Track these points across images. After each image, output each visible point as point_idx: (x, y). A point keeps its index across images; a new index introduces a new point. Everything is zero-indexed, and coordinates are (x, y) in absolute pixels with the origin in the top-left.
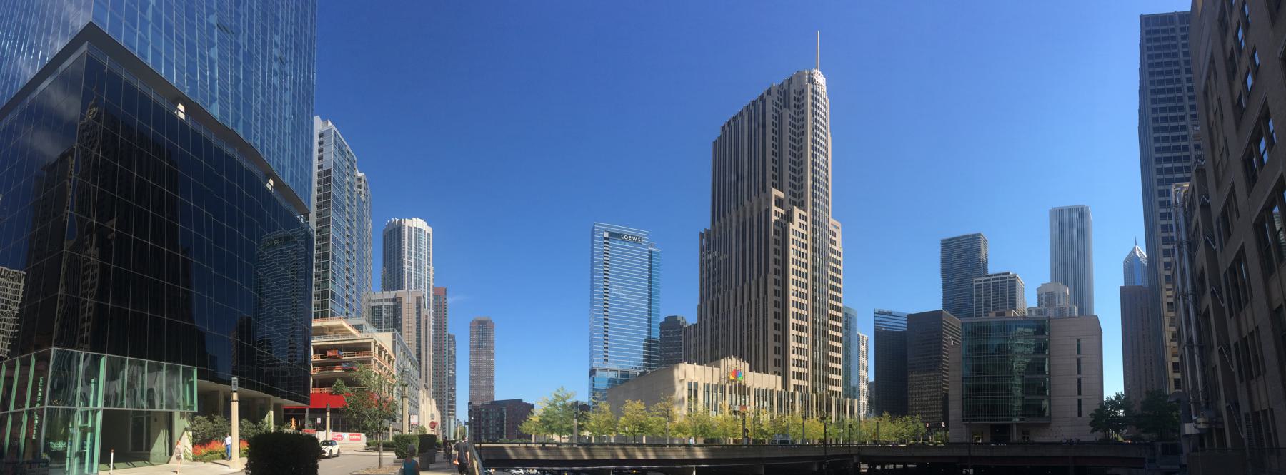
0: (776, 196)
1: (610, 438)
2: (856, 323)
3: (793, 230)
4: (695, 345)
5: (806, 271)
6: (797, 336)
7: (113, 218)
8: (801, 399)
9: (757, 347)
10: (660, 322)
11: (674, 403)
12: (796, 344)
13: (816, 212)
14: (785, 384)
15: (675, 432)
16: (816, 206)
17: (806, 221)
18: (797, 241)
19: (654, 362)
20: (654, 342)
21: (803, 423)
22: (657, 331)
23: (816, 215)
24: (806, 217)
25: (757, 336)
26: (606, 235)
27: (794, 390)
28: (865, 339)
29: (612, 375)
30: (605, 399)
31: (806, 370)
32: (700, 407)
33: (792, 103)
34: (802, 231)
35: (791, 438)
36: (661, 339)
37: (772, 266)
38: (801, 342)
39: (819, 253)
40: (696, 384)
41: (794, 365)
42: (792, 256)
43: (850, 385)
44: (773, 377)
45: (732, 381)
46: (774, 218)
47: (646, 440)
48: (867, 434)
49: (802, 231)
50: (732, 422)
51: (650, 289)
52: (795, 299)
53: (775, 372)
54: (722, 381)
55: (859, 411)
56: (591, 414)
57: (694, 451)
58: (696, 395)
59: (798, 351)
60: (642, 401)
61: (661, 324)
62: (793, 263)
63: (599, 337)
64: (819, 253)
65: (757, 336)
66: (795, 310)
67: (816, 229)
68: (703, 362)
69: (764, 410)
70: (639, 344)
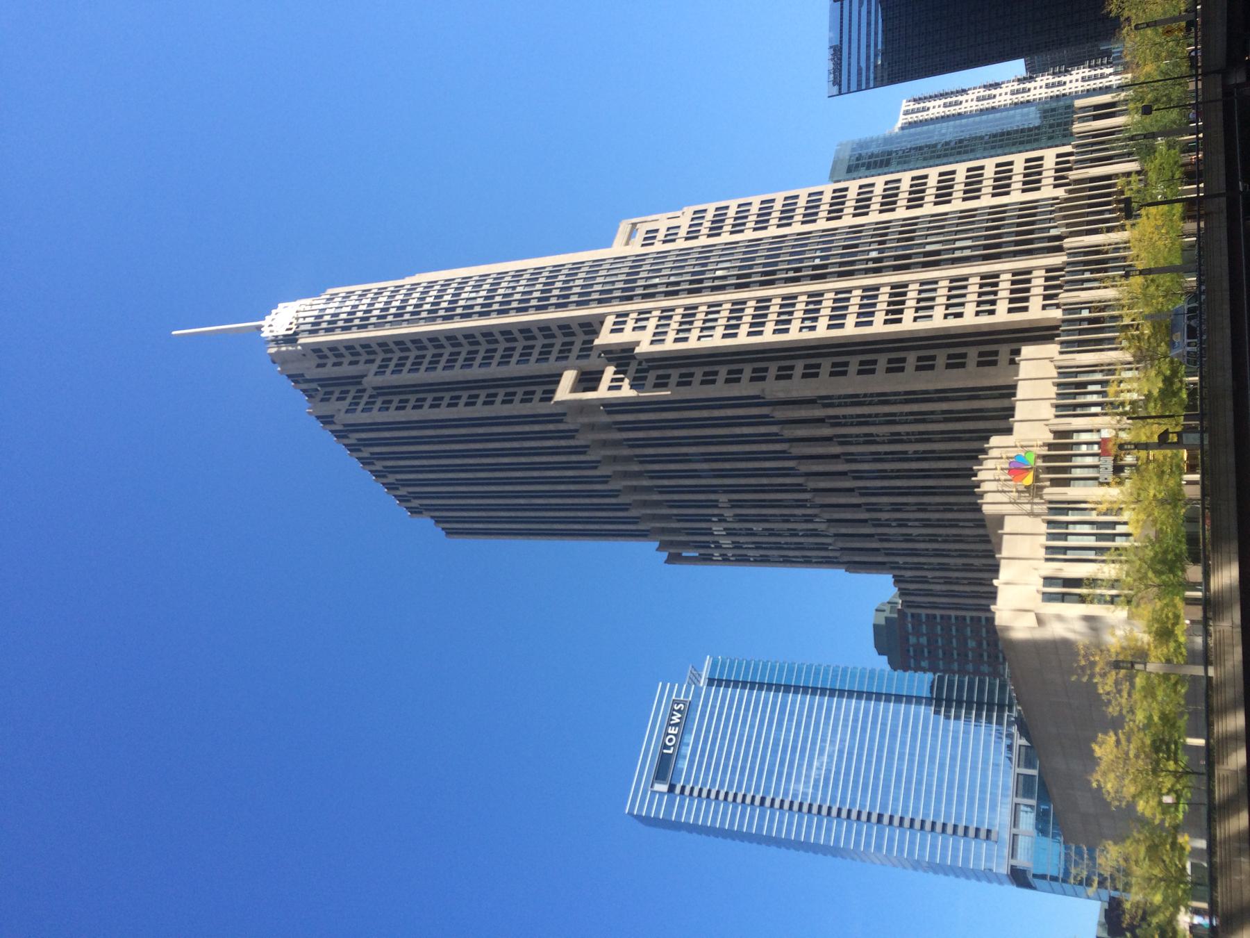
0: (574, 389)
1: (1195, 852)
2: (872, 141)
3: (652, 342)
4: (948, 581)
5: (753, 303)
6: (917, 310)
8: (1079, 284)
9: (950, 416)
10: (888, 668)
11: (1099, 647)
12: (939, 312)
13: (601, 292)
14: (1041, 334)
15: (1172, 645)
16: (589, 294)
17: (626, 315)
18: (679, 331)
19: (991, 692)
20: (940, 688)
21: (1142, 272)
22: (911, 681)
23: (610, 291)
24: (618, 315)
25: (921, 418)
26: (664, 788)
27: (1058, 306)
28: (912, 106)
29: (1028, 820)
30: (1091, 851)
31: (1003, 277)
32: (1108, 571)
33: (346, 370)
34: (652, 324)
35: (1182, 303)
36: (933, 669)
37: (745, 388)
38: (933, 299)
39: (703, 273)
40: (1049, 581)
41: (992, 312)
42: (717, 340)
43: (1038, 128)
44: (1025, 369)
45: (1037, 479)
46: (627, 391)
47: (1197, 736)
48: (1172, 54)
49: (652, 324)
50: (1142, 478)
51: (805, 690)
52: (823, 323)
53: (1012, 362)
54: (1037, 509)
55: (1107, 90)
56: (1133, 898)
57: (1221, 593)
58: (1077, 582)
59: (954, 306)
60: (1094, 740)
61: (894, 665)
62: (735, 335)
63: (926, 846)
64: (703, 273)
65: (921, 418)
66: (851, 320)
67: (646, 287)
68: (990, 561)
69: (1111, 389)
70: (946, 730)
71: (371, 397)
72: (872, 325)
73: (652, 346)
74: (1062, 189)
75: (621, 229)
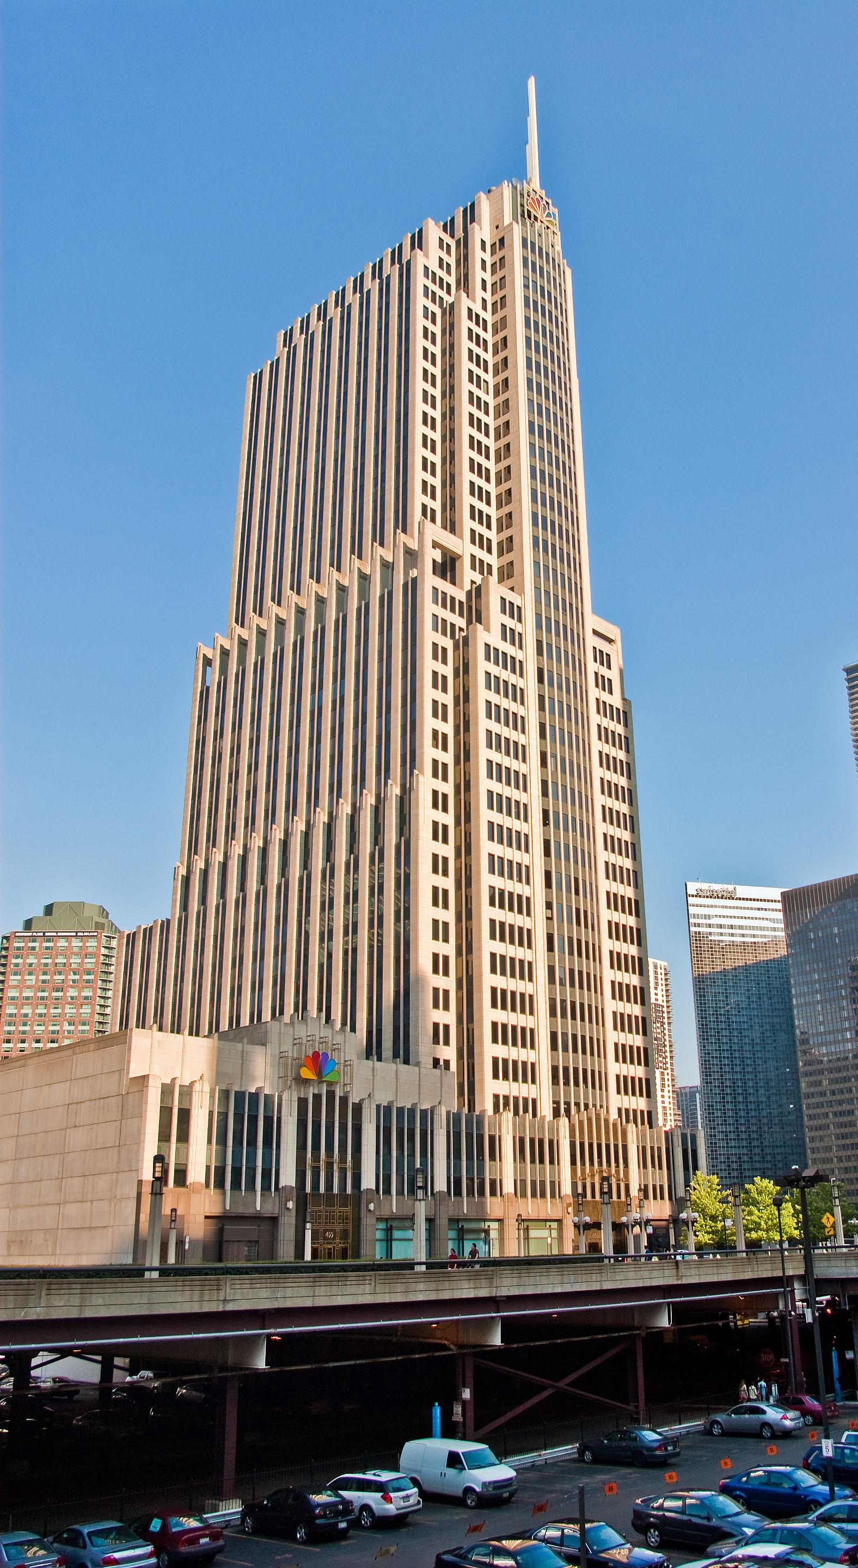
3: (487, 646)
7: (502, 1453)
63: (61, 1164)
71: (441, 299)
72: (488, 808)
73: (487, 823)
74: (616, 1116)
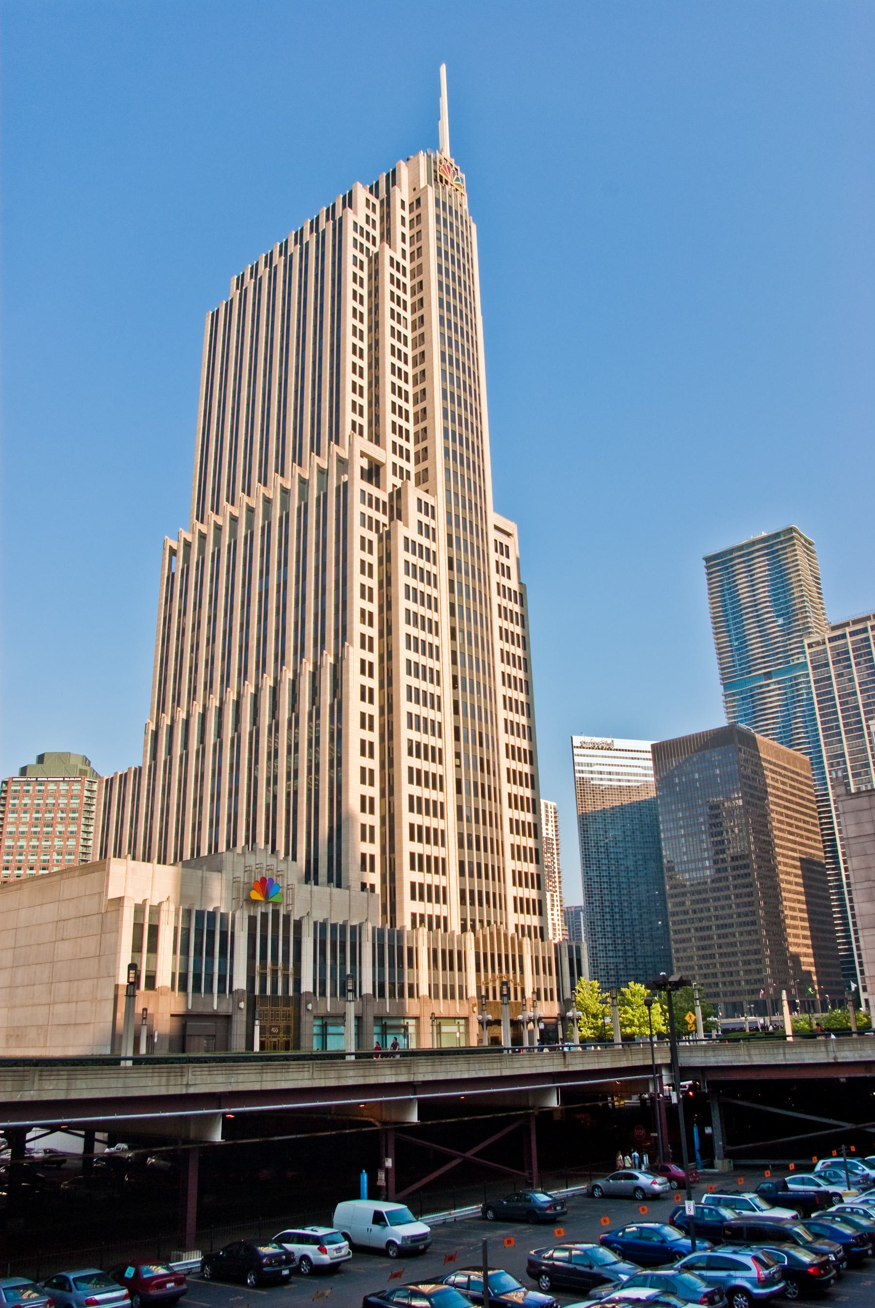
3: (406, 539)
74: (514, 931)
75: (509, 522)
